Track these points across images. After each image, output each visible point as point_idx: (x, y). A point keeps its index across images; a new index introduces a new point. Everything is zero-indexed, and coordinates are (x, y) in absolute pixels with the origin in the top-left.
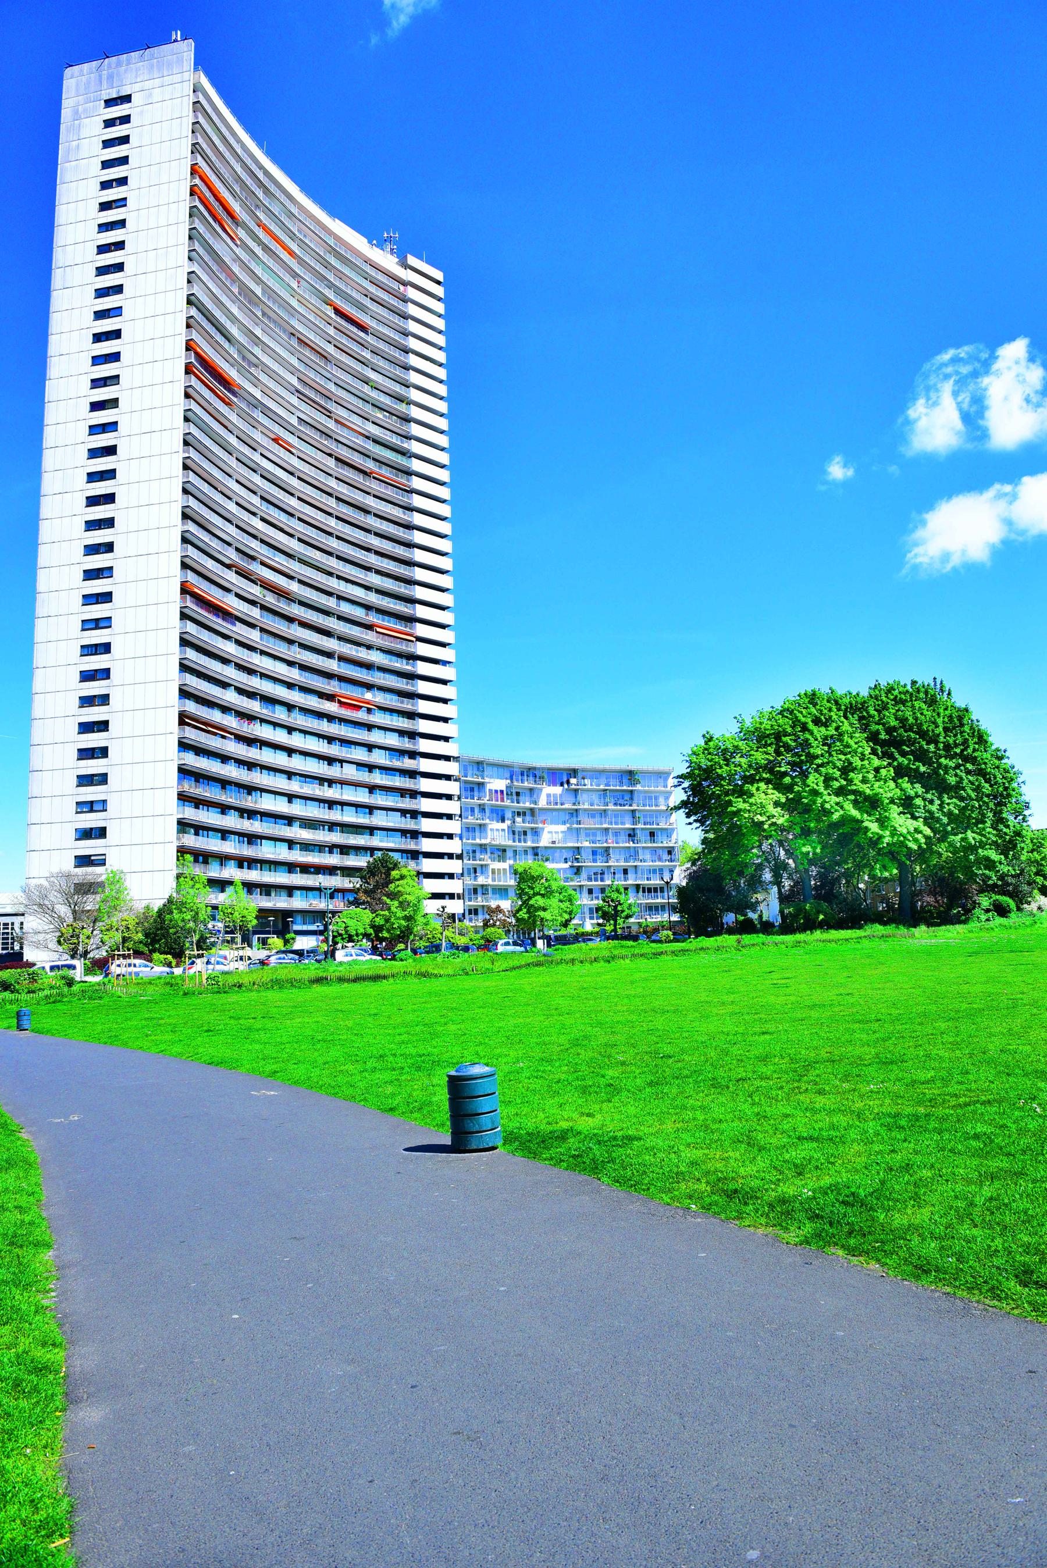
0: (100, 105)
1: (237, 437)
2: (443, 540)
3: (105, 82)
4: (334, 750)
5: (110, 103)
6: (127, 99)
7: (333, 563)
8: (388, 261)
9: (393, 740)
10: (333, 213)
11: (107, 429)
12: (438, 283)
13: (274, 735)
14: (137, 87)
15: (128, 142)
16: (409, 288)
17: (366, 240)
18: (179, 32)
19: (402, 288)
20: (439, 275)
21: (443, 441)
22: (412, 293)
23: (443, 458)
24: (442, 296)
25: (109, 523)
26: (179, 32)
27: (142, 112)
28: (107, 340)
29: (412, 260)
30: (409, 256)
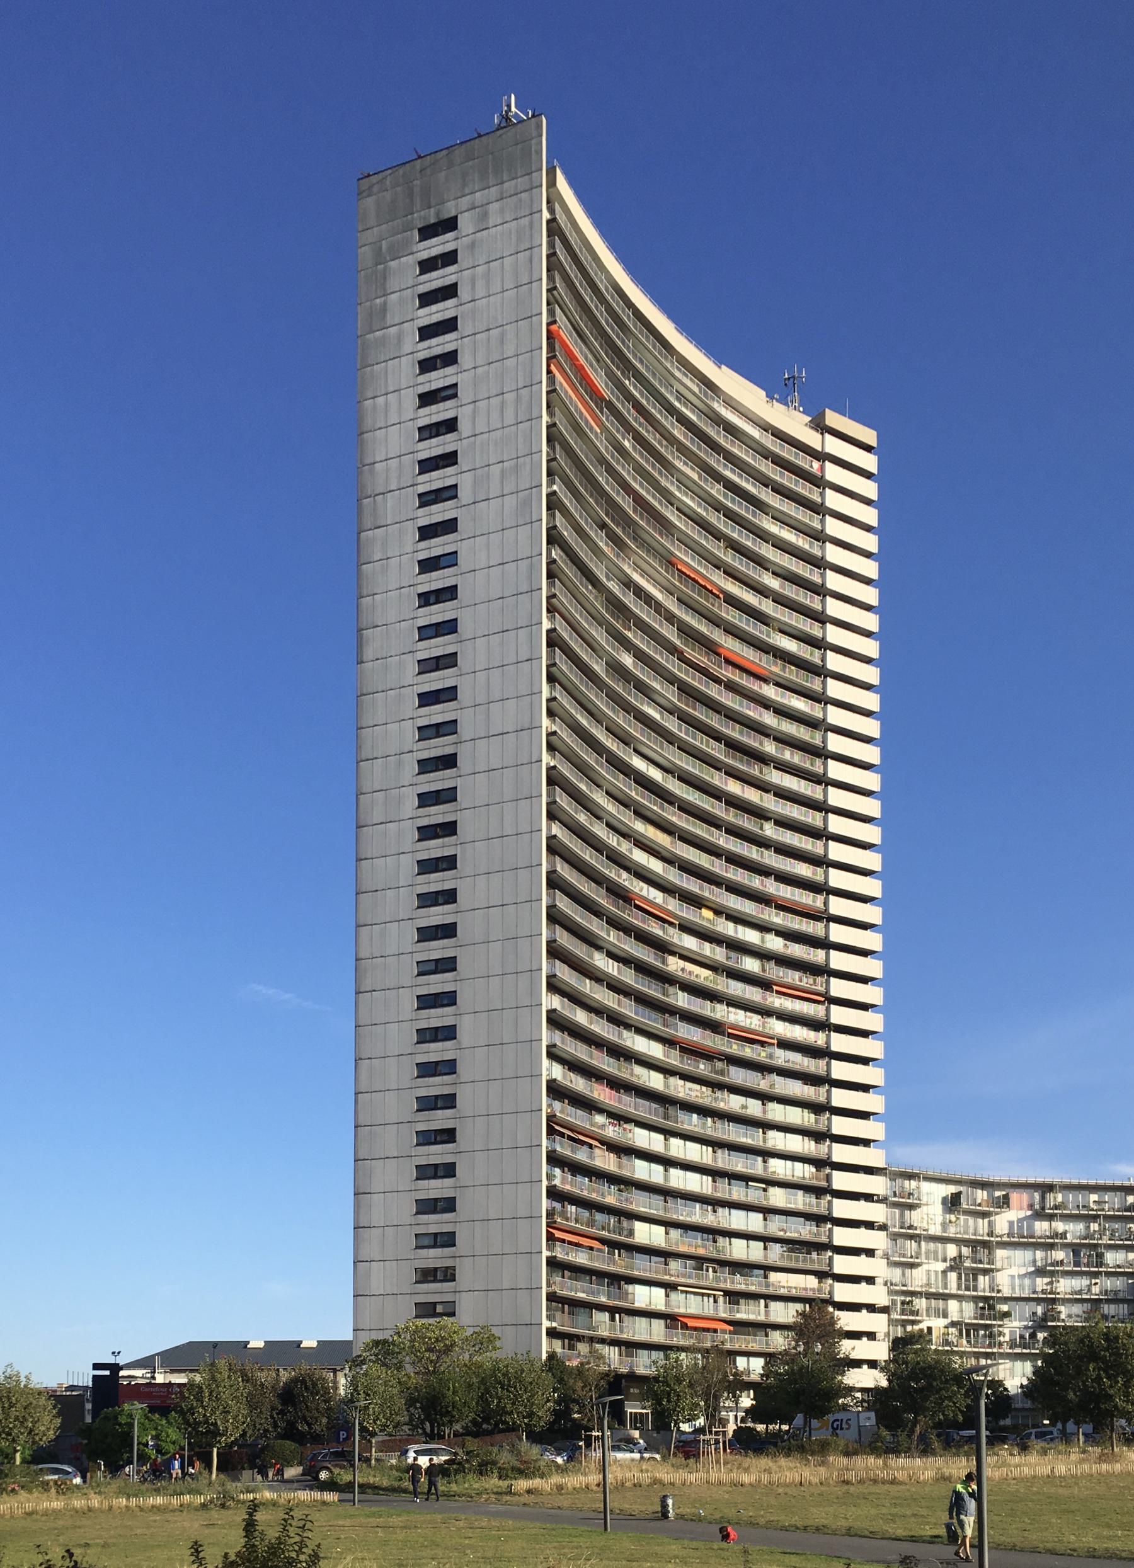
0: (412, 236)
1: (607, 793)
2: (867, 825)
3: (418, 201)
4: (693, 885)
5: (428, 232)
6: (450, 224)
7: (718, 867)
8: (795, 424)
9: (803, 1172)
10: (720, 359)
11: (442, 730)
12: (868, 448)
13: (665, 1209)
14: (464, 202)
15: (455, 328)
16: (828, 465)
17: (764, 393)
18: (513, 97)
19: (816, 465)
20: (869, 436)
21: (871, 701)
22: (833, 473)
23: (871, 701)
24: (874, 470)
25: (450, 863)
26: (513, 97)
27: (473, 245)
28: (437, 602)
29: (833, 419)
30: (827, 410)
